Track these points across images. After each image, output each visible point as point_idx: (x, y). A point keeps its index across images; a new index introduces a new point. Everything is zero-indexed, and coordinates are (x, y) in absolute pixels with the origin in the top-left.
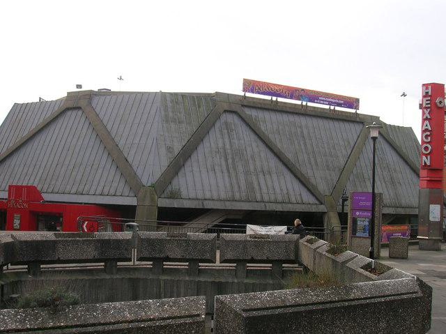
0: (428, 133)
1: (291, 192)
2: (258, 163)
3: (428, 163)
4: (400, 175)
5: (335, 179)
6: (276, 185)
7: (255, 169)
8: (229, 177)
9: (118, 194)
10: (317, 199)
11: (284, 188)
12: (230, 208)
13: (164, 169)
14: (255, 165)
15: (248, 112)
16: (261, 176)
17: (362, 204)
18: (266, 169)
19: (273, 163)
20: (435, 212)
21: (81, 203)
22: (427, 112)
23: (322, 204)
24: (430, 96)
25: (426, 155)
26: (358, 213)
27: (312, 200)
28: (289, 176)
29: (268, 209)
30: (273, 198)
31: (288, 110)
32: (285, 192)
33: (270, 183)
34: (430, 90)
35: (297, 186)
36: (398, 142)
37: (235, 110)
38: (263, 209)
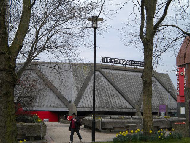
0: (178, 84)
1: (122, 104)
2: (109, 92)
3: (178, 94)
4: (163, 95)
5: (138, 98)
6: (117, 101)
7: (108, 95)
8: (99, 98)
9: (45, 106)
10: (132, 106)
11: (119, 102)
12: (102, 111)
13: (76, 96)
14: (108, 93)
15: (103, 70)
16: (111, 98)
17: (162, 108)
18: (112, 94)
19: (115, 92)
20: (183, 111)
21: (42, 111)
22: (178, 77)
23: (134, 108)
24: (179, 72)
25: (178, 91)
26: (161, 111)
27: (128, 106)
28: (121, 97)
29: (115, 111)
30: (87, 106)
31: (119, 69)
32: (120, 104)
33: (114, 101)
34: (178, 70)
35: (124, 101)
36: (163, 80)
37: (99, 70)
38: (113, 111)
